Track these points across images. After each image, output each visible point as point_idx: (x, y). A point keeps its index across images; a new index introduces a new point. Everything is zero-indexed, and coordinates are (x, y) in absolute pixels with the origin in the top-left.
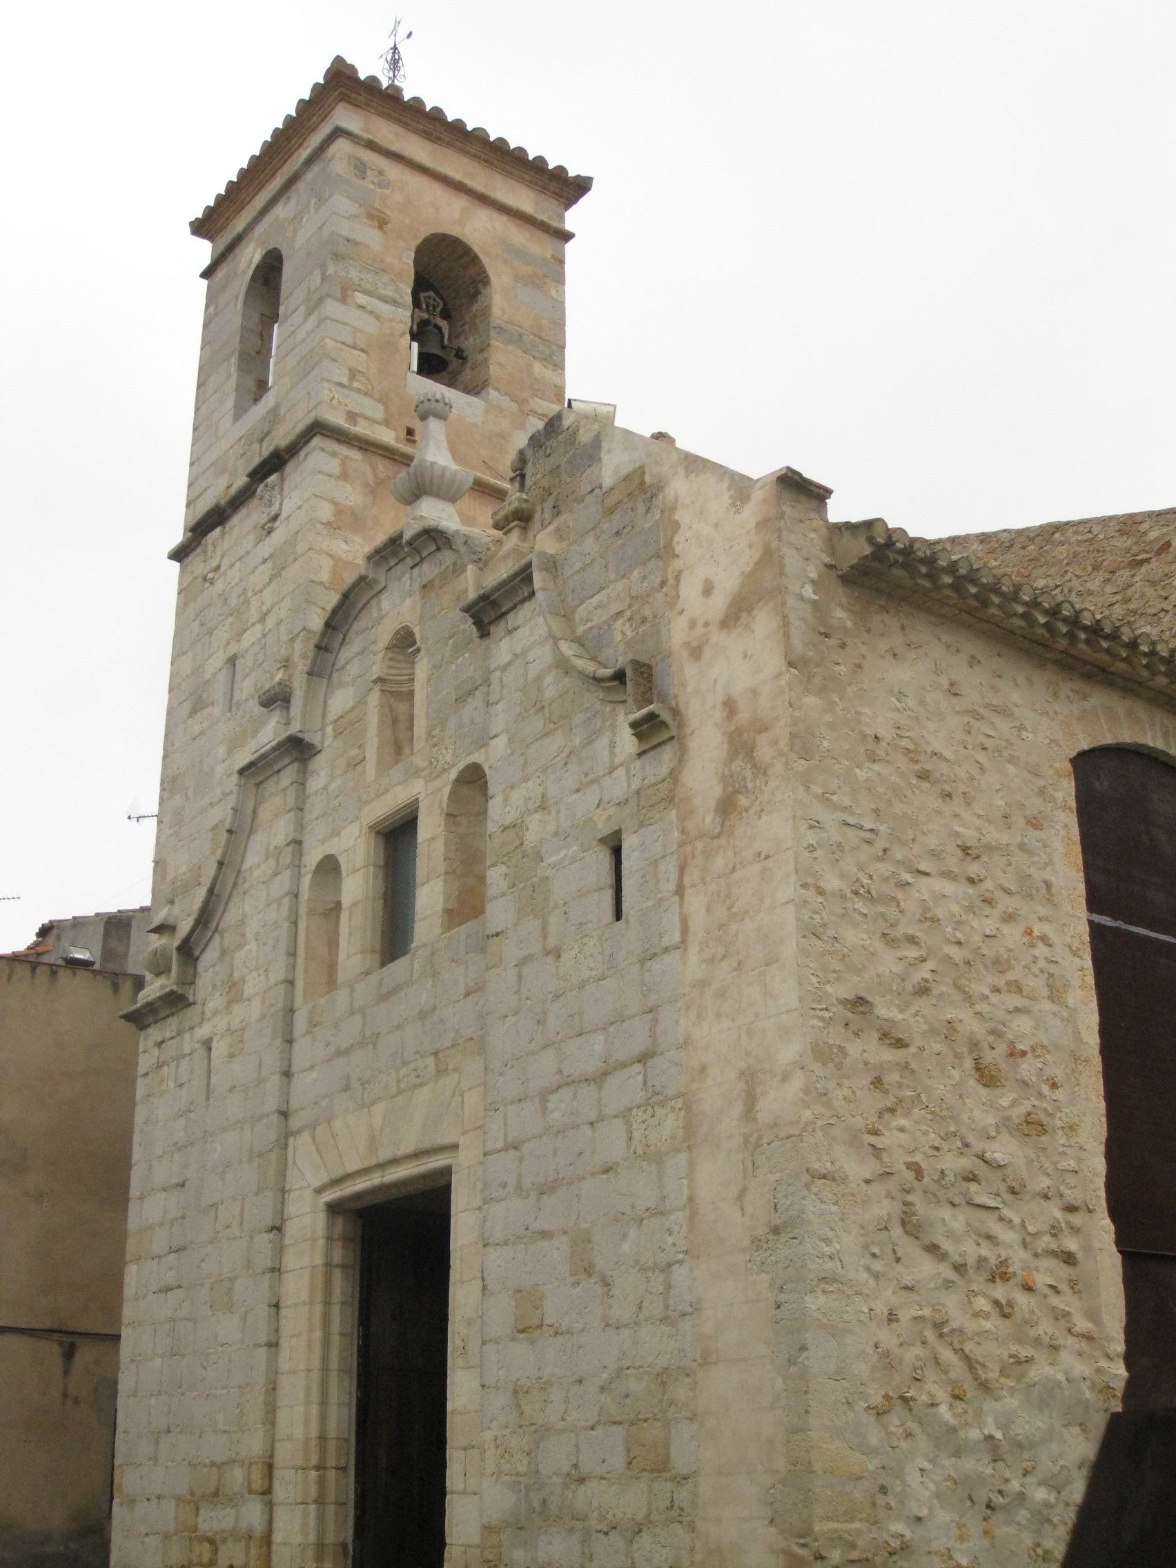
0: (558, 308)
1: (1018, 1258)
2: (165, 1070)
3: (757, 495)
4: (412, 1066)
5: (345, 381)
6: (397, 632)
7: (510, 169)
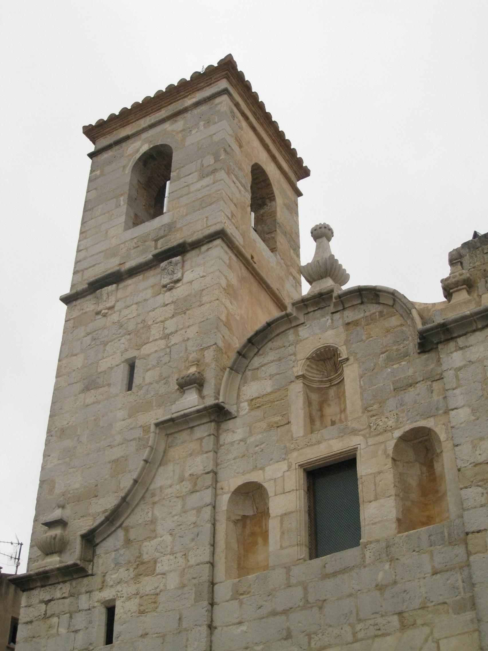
2: (55, 620)
4: (372, 622)
6: (329, 347)
7: (282, 150)
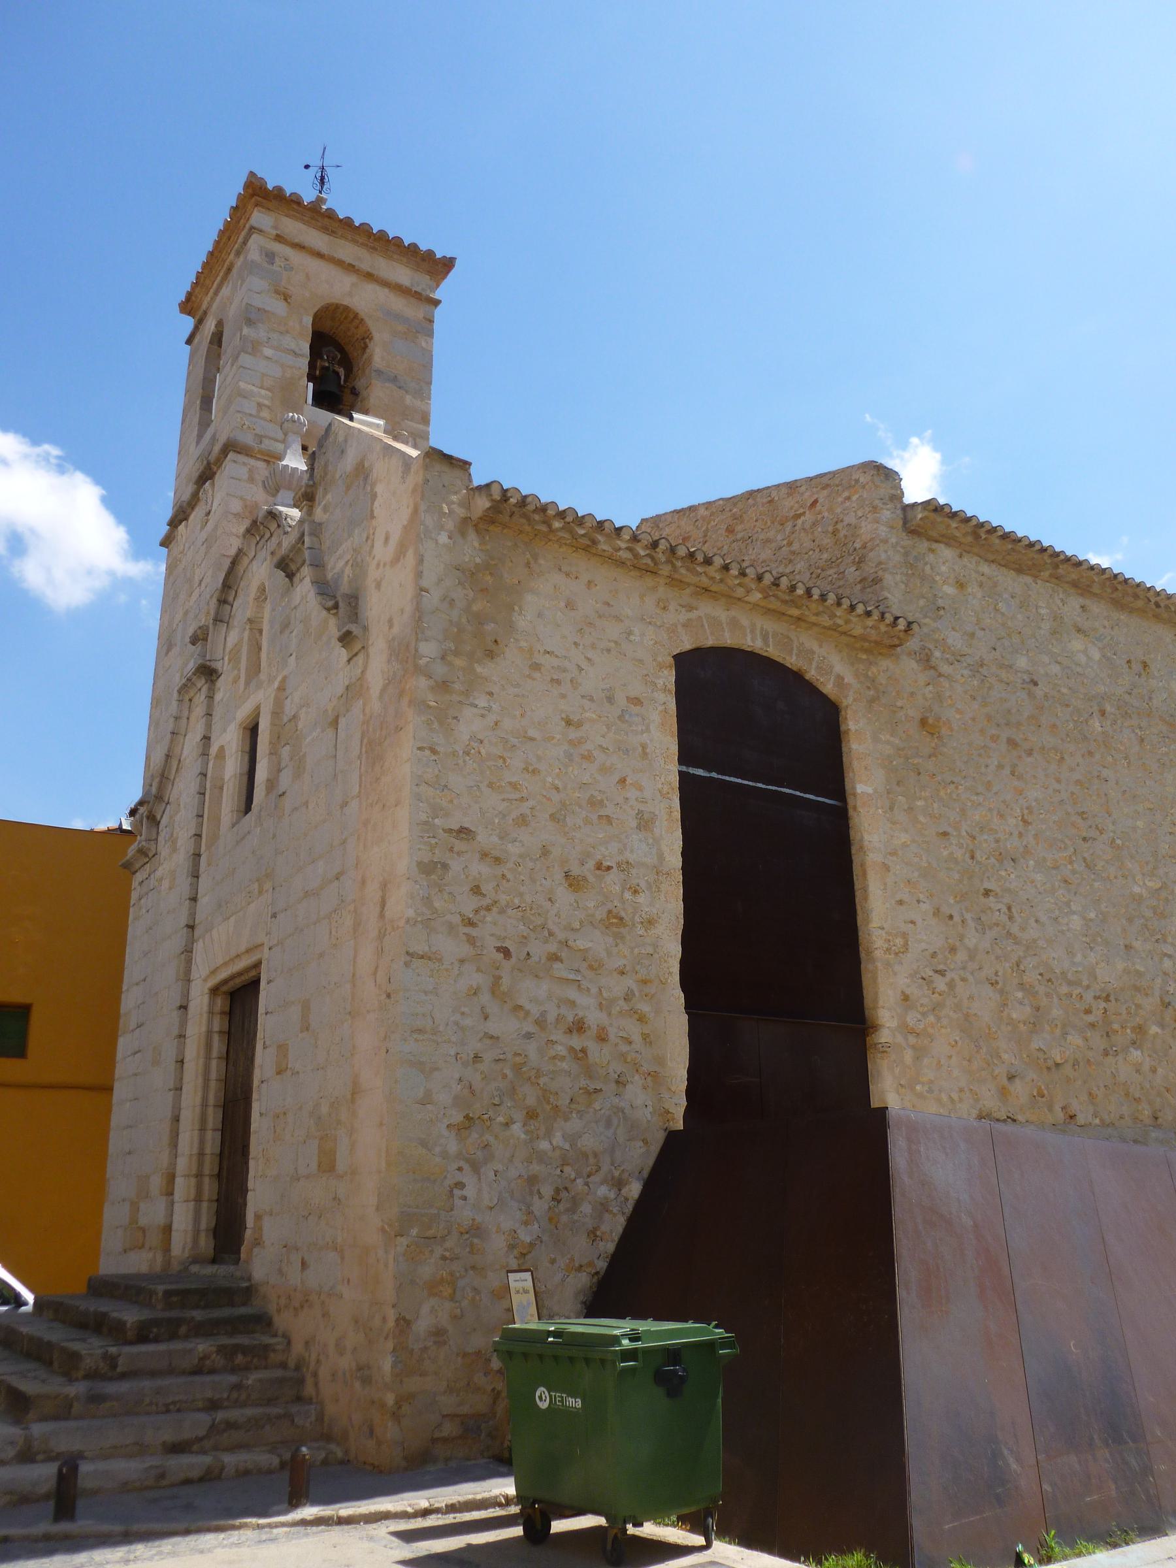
0: (428, 356)
1: (594, 1018)
3: (414, 468)
5: (254, 412)
